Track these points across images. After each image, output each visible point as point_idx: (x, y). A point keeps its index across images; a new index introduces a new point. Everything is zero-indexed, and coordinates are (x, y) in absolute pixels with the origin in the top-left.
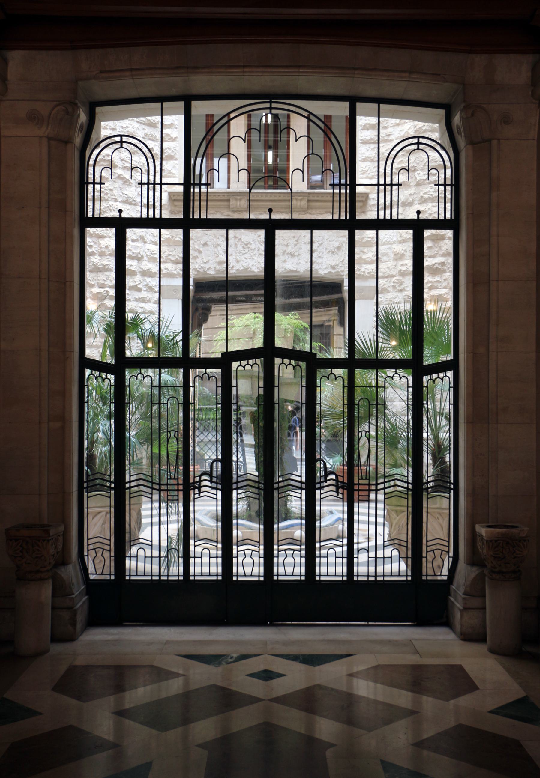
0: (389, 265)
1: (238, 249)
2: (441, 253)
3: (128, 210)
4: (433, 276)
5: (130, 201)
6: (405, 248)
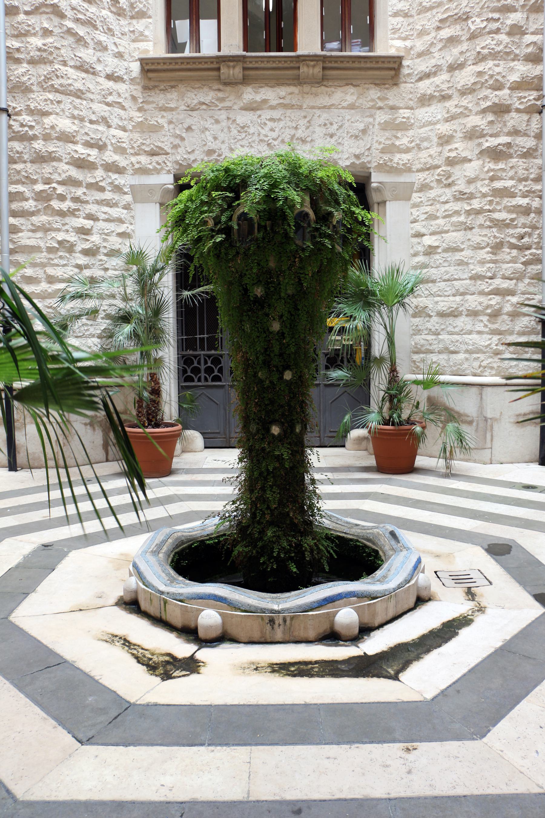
0: (432, 153)
1: (232, 134)
2: (506, 130)
3: (83, 79)
4: (495, 163)
5: (85, 67)
6: (454, 127)
